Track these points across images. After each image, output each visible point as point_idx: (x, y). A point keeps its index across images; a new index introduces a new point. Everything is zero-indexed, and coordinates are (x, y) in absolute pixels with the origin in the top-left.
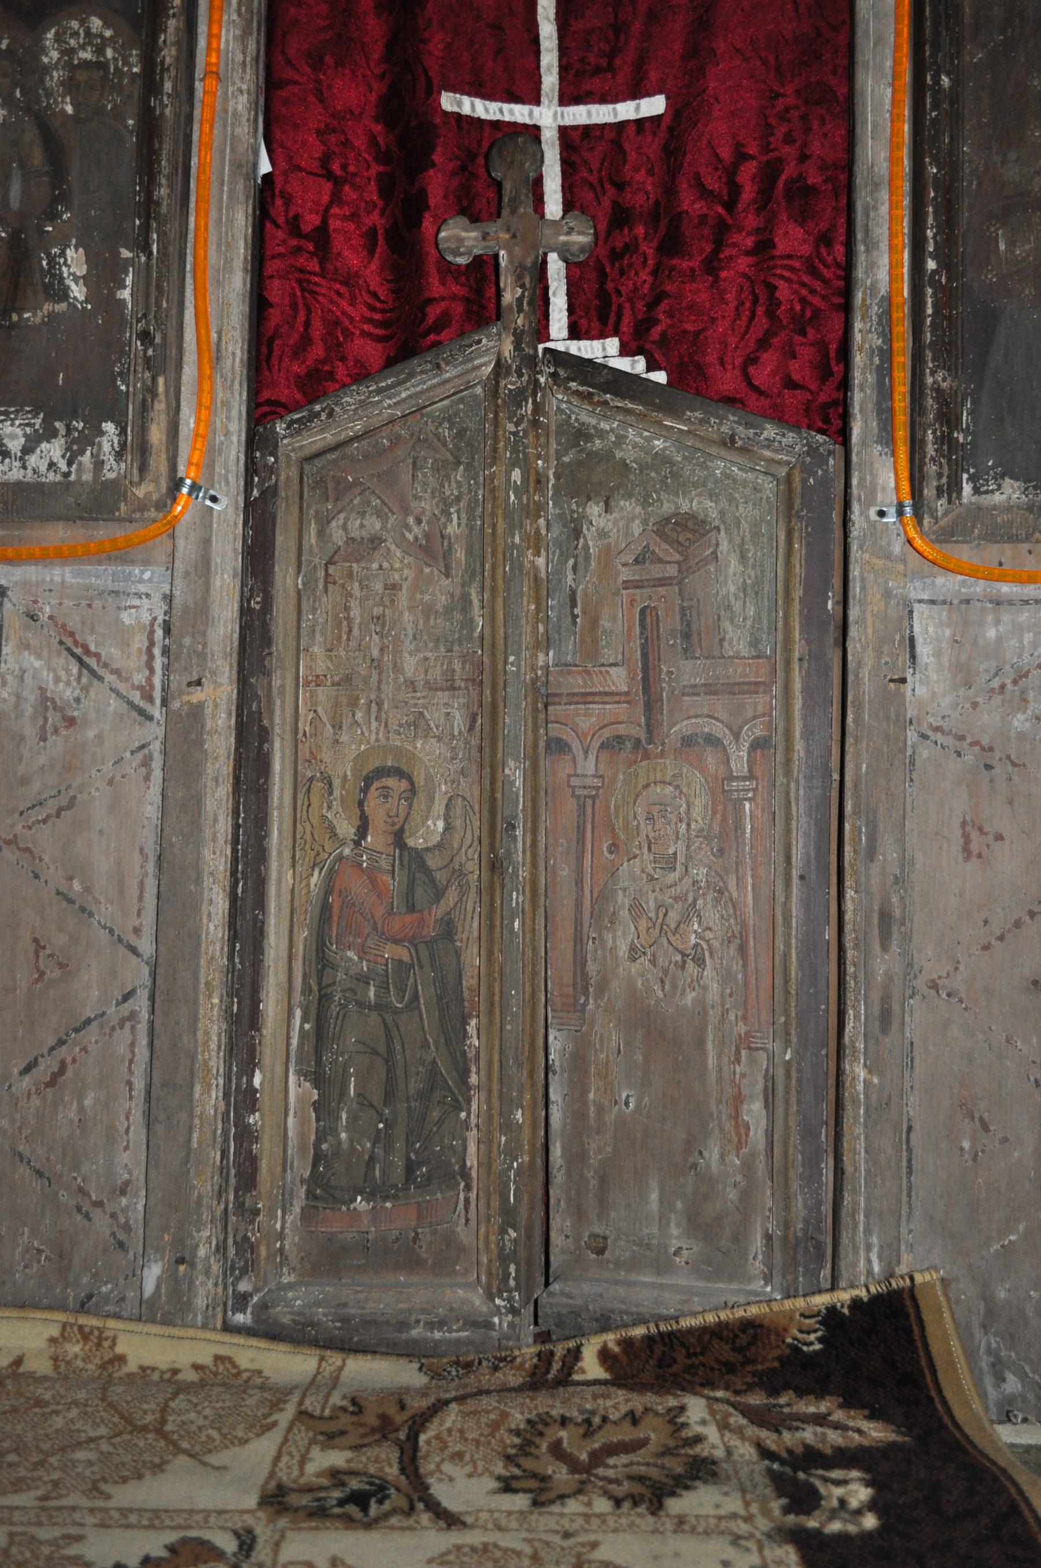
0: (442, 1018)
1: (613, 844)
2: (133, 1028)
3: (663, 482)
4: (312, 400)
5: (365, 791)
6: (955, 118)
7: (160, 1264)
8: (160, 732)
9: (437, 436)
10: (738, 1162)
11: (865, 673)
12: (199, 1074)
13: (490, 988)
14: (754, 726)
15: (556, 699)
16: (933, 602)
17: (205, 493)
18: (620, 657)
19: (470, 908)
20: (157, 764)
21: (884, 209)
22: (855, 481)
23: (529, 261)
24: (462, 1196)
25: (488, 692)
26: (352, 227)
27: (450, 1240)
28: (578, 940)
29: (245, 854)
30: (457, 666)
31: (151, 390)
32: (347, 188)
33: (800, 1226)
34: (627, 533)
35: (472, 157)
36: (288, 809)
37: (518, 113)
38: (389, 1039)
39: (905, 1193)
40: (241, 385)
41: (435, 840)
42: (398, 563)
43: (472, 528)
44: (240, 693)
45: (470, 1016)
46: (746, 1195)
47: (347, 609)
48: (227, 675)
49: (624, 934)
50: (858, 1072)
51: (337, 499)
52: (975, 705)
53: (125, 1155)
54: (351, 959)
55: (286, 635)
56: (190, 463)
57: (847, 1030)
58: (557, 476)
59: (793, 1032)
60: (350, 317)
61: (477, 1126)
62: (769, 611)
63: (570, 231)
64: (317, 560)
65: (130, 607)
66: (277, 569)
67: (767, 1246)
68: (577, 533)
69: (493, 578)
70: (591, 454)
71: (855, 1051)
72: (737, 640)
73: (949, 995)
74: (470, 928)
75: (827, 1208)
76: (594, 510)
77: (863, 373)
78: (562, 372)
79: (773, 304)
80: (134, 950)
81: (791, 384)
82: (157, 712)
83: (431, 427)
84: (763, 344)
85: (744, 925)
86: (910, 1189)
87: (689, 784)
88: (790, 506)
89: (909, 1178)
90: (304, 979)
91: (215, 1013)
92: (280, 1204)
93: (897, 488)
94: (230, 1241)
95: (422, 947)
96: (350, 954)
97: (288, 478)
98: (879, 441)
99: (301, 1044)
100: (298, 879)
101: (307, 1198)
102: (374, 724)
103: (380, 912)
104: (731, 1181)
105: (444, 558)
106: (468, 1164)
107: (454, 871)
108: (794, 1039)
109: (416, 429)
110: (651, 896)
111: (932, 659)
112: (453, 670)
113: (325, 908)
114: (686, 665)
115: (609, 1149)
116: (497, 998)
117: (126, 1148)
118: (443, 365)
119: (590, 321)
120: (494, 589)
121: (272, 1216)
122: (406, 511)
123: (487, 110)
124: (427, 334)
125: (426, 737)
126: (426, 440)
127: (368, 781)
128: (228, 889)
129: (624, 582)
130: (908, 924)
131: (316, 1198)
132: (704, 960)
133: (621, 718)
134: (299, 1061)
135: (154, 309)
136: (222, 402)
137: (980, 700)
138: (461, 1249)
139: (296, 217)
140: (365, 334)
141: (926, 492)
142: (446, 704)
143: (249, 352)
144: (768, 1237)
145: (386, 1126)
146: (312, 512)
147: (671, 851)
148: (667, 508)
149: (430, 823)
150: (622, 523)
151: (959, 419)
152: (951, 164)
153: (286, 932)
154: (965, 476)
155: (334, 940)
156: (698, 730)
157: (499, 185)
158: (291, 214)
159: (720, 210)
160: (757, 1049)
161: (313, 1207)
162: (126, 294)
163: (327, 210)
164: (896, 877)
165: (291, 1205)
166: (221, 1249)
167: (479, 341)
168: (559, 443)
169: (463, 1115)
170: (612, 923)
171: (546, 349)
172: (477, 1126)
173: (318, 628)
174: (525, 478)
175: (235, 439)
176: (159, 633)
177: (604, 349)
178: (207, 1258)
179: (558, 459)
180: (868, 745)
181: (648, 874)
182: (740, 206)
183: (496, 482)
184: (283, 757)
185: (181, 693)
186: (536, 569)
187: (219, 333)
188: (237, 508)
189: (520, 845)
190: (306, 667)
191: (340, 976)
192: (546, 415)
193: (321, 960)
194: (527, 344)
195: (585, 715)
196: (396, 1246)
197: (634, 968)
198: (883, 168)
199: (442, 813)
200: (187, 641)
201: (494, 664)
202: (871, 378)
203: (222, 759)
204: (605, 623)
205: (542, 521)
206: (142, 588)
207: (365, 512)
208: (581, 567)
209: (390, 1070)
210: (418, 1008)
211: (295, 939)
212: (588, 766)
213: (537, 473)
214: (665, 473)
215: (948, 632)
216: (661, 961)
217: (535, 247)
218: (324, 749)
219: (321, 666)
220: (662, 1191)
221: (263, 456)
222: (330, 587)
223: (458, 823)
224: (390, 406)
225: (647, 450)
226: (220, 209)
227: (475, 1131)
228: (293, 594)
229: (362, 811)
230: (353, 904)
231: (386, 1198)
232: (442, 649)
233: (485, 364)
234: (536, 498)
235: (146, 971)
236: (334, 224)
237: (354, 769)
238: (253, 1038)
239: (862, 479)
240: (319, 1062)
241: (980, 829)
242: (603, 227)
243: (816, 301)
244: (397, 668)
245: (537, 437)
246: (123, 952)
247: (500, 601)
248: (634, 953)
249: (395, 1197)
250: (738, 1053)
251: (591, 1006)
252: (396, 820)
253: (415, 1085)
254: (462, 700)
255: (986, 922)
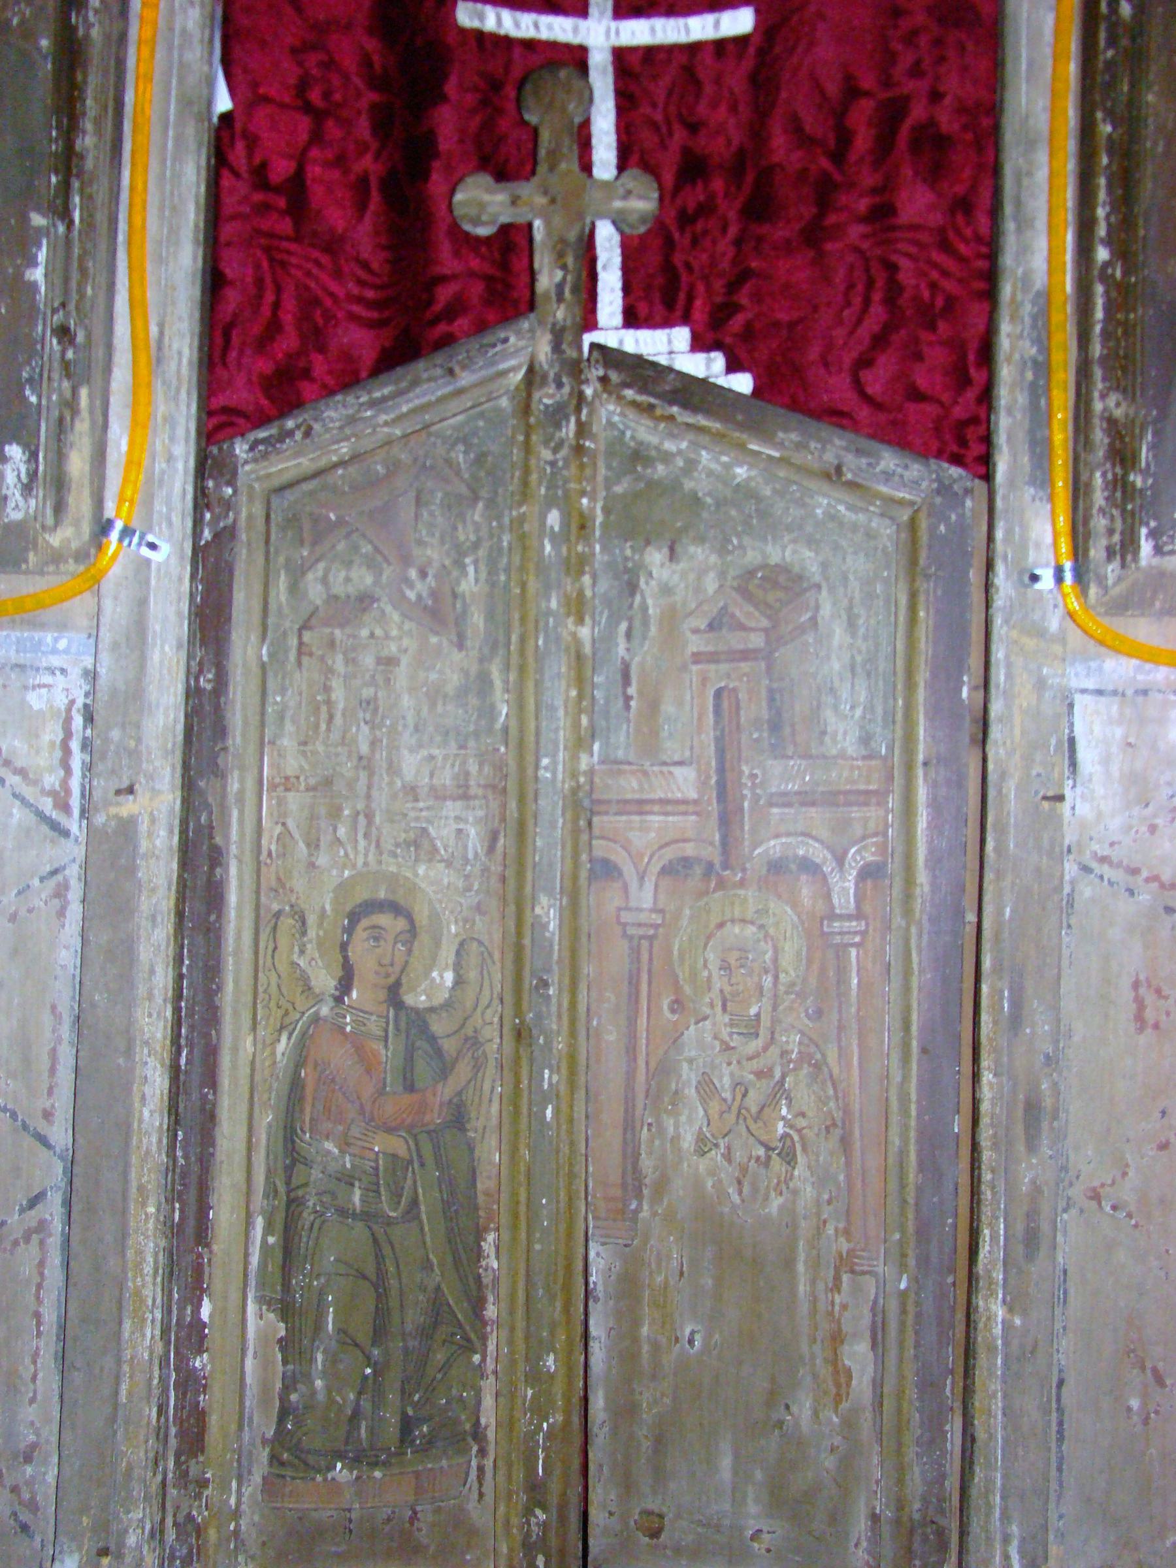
0: (450, 1230)
1: (676, 1001)
2: (42, 1243)
3: (747, 523)
4: (282, 414)
5: (350, 930)
6: (1136, 59)
7: (76, 1556)
8: (80, 852)
9: (448, 462)
10: (835, 1419)
11: (1011, 787)
12: (129, 1306)
13: (514, 1194)
14: (865, 848)
15: (603, 808)
16: (1100, 692)
17: (142, 538)
18: (687, 754)
19: (487, 1086)
20: (75, 893)
21: (1042, 175)
22: (999, 534)
23: (572, 236)
24: (474, 1463)
25: (513, 805)
26: (336, 175)
27: (458, 1521)
28: (629, 1126)
29: (191, 1013)
30: (473, 768)
31: (71, 405)
32: (330, 123)
33: (917, 1505)
34: (698, 590)
35: (496, 86)
36: (247, 954)
37: (556, 28)
38: (379, 1258)
39: (1054, 1465)
40: (189, 394)
41: (442, 996)
42: (395, 631)
43: (493, 585)
44: (186, 802)
45: (486, 1230)
46: (848, 1462)
47: (327, 689)
48: (167, 779)
49: (690, 1120)
50: (994, 1310)
51: (315, 543)
52: (1153, 829)
53: (30, 1410)
54: (329, 1152)
55: (246, 723)
56: (121, 500)
57: (981, 1256)
58: (607, 511)
59: (910, 1253)
60: (332, 295)
61: (495, 1372)
62: (885, 697)
63: (628, 194)
64: (287, 624)
65: (40, 686)
66: (234, 636)
67: (873, 1529)
68: (632, 588)
69: (522, 652)
70: (651, 484)
71: (991, 1282)
72: (843, 732)
73: (1114, 1208)
74: (488, 1113)
75: (952, 1483)
76: (655, 557)
77: (1012, 392)
78: (614, 377)
79: (894, 290)
80: (43, 1141)
81: (916, 395)
82: (74, 825)
83: (441, 450)
84: (880, 341)
85: (847, 1112)
86: (1061, 1459)
87: (777, 924)
88: (913, 562)
89: (1059, 1447)
90: (267, 1178)
91: (151, 1225)
92: (235, 1472)
93: (1055, 544)
94: (169, 1521)
95: (423, 1137)
96: (329, 1145)
97: (250, 517)
98: (1032, 482)
99: (263, 1264)
100: (259, 1046)
101: (271, 1464)
102: (362, 843)
103: (368, 1091)
104: (826, 1443)
105: (457, 624)
106: (483, 1421)
107: (466, 1039)
108: (912, 1262)
109: (421, 453)
110: (726, 1070)
111: (1098, 768)
112: (467, 774)
113: (296, 1086)
114: (776, 767)
115: (667, 1400)
116: (523, 1209)
117: (32, 1400)
118: (457, 370)
119: (651, 304)
120: (522, 669)
121: (225, 1487)
122: (406, 560)
123: (517, 25)
124: (436, 320)
125: (430, 860)
126: (432, 468)
127: (354, 917)
128: (168, 1062)
129: (694, 654)
130: (1062, 1115)
131: (282, 1464)
132: (795, 1155)
133: (690, 834)
134: (261, 1285)
135: (75, 296)
136: (165, 419)
137: (1159, 821)
138: (473, 1532)
139: (264, 166)
140: (352, 317)
141: (1092, 553)
142: (458, 819)
143: (200, 349)
144: (875, 1518)
145: (375, 1372)
146: (281, 559)
147: (753, 1011)
148: (752, 557)
149: (435, 974)
150: (692, 576)
151: (1135, 457)
152: (1130, 121)
153: (245, 1116)
154: (1144, 531)
155: (307, 1127)
156: (790, 853)
157: (535, 133)
158: (257, 161)
159: (825, 163)
160: (864, 1273)
161: (279, 1476)
162: (37, 275)
163: (305, 151)
164: (1047, 1056)
165: (250, 1472)
166: (157, 1533)
167: (506, 340)
168: (609, 467)
169: (477, 1358)
170: (673, 1104)
171: (594, 346)
172: (495, 1372)
173: (289, 714)
174: (565, 523)
175: (180, 466)
176: (78, 721)
177: (670, 342)
178: (139, 1547)
179: (608, 488)
180: (1013, 883)
181: (723, 1042)
182: (853, 157)
183: (526, 527)
184: (240, 887)
185: (107, 804)
186: (577, 642)
187: (161, 326)
188: (182, 558)
189: (554, 1009)
190: (271, 766)
191: (316, 1174)
192: (593, 437)
193: (291, 1154)
194: (570, 344)
195: (641, 829)
196: (387, 1528)
197: (703, 1165)
198: (1041, 122)
199: (451, 961)
200: (115, 734)
201: (522, 769)
202: (1022, 399)
203: (162, 892)
204: (668, 708)
205: (587, 580)
206: (56, 661)
207: (351, 562)
208: (637, 632)
209: (381, 1296)
210: (417, 1217)
211: (255, 1123)
212: (644, 897)
213: (581, 515)
214: (748, 511)
215: (1119, 732)
216: (739, 1155)
217: (581, 216)
218: (295, 874)
219: (292, 764)
220: (736, 1455)
221: (218, 486)
222: (305, 660)
223: (472, 975)
224: (386, 424)
225: (725, 478)
226: (164, 161)
227: (492, 1378)
228: (255, 669)
229: (346, 958)
230: (333, 1080)
231: (374, 1465)
232: (453, 744)
233: (514, 369)
234: (580, 548)
235: (59, 1168)
236: (315, 171)
237: (335, 901)
238: (200, 1256)
239: (1009, 532)
240: (286, 1286)
241: (1158, 991)
242: (669, 178)
243: (948, 285)
244: (393, 769)
245: (582, 466)
246: (28, 1141)
247: (530, 685)
248: (703, 1145)
249: (385, 1464)
250: (837, 1279)
251: (645, 1214)
252: (390, 969)
253: (414, 1318)
254: (480, 813)
255: (1163, 1113)
